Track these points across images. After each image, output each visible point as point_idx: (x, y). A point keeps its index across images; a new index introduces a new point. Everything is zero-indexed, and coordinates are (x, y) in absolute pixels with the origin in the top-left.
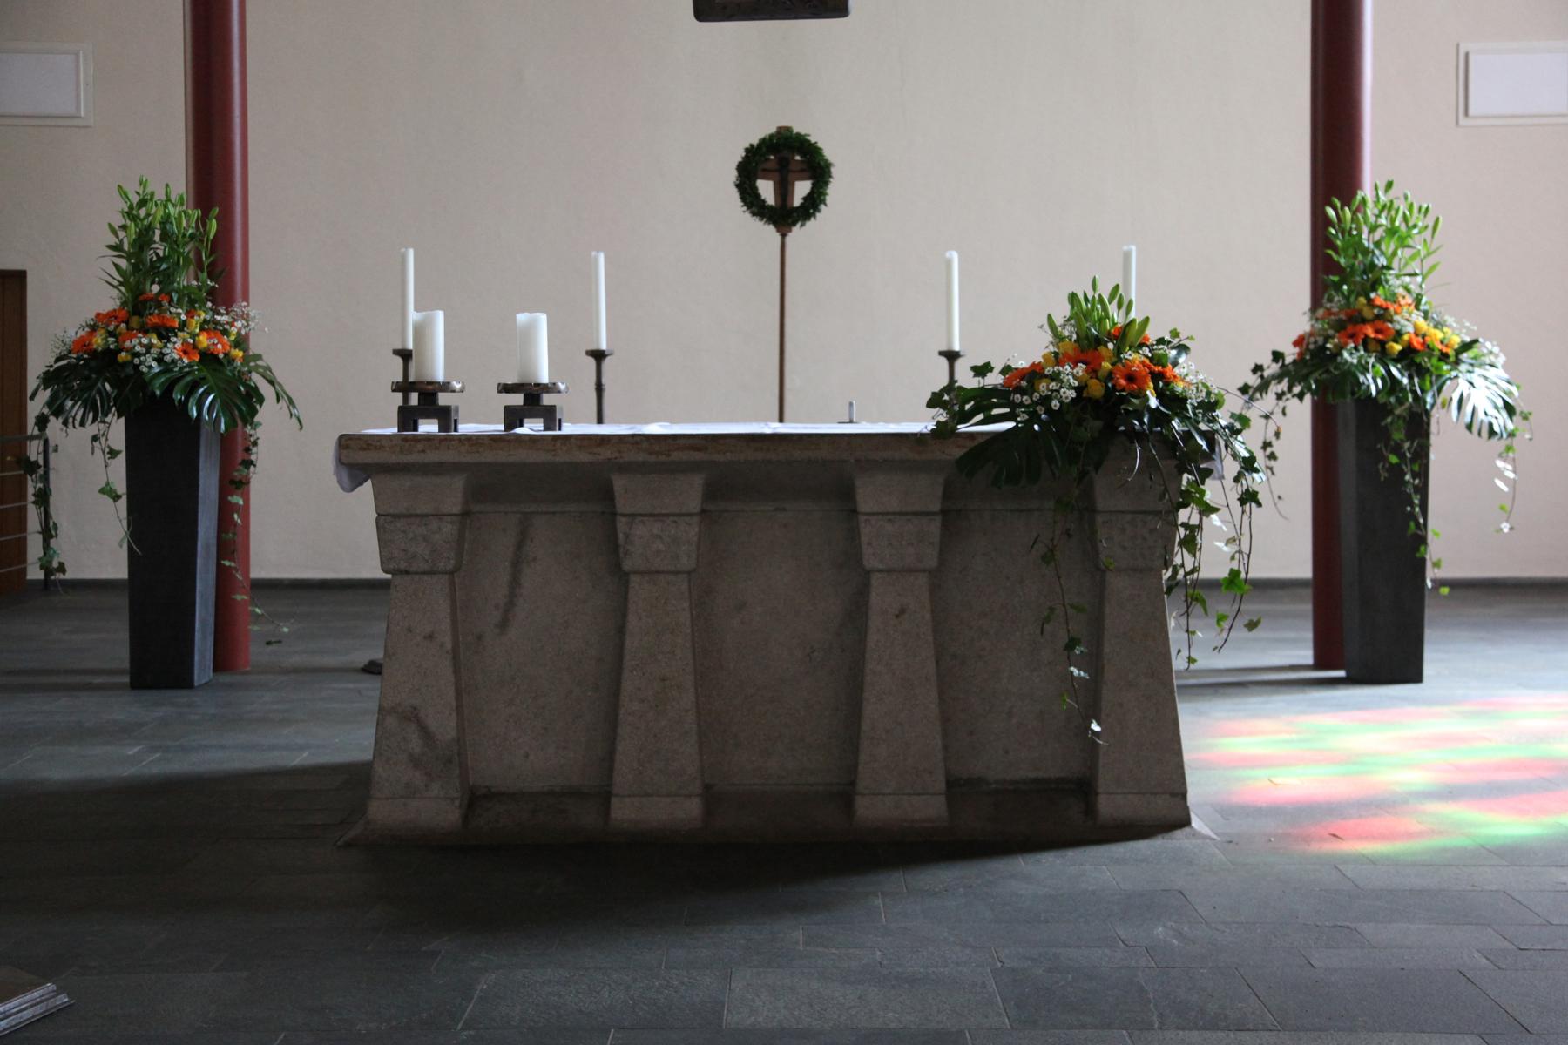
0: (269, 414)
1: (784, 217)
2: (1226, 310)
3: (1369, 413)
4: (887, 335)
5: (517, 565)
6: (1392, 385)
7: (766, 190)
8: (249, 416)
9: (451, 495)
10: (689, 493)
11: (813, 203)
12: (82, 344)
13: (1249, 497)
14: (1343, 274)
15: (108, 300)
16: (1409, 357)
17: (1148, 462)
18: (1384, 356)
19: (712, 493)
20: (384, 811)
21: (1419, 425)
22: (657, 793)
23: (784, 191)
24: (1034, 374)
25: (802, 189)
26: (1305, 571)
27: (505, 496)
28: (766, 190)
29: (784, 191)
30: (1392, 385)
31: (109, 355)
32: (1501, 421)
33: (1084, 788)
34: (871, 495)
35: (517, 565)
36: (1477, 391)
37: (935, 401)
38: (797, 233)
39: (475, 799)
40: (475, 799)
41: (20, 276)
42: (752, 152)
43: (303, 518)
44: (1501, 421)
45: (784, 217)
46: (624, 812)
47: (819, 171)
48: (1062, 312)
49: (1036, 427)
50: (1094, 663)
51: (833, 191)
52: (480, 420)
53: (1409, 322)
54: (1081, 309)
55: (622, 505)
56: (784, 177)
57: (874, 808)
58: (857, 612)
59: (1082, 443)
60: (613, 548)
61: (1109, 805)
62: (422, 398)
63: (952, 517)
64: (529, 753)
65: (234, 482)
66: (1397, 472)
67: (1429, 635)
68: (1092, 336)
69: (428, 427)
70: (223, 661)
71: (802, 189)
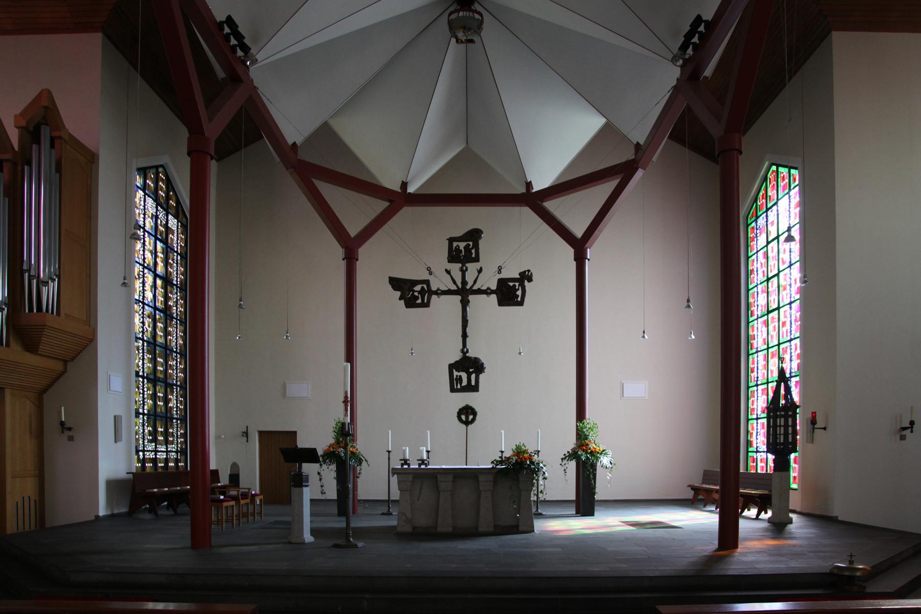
0: (364, 463)
1: (467, 423)
2: (551, 447)
3: (584, 462)
4: (485, 450)
5: (421, 489)
6: (587, 458)
7: (463, 417)
8: (360, 464)
9: (410, 478)
10: (450, 477)
11: (473, 420)
12: (328, 450)
13: (545, 478)
14: (581, 436)
15: (332, 441)
16: (592, 453)
17: (527, 473)
18: (587, 453)
19: (454, 477)
20: (399, 529)
21: (594, 466)
22: (445, 526)
23: (467, 418)
24: (509, 458)
25: (471, 417)
26: (574, 498)
27: (418, 479)
28: (463, 417)
29: (467, 418)
30: (587, 458)
31: (334, 452)
32: (609, 465)
33: (517, 526)
34: (481, 478)
35: (421, 489)
36: (605, 460)
37: (492, 462)
38: (470, 426)
39: (414, 528)
40: (414, 528)
41: (295, 432)
42: (460, 410)
43: (373, 482)
44: (609, 465)
45: (467, 423)
46: (439, 529)
47: (474, 413)
48: (514, 448)
49: (222, 497)
50: (519, 505)
51: (478, 417)
52: (414, 466)
53: (592, 446)
54: (518, 447)
55: (439, 479)
56: (467, 415)
57: (481, 529)
58: (479, 497)
59: (519, 470)
60: (437, 487)
61: (521, 529)
62: (405, 462)
63: (495, 482)
64: (423, 521)
65: (356, 477)
66: (589, 475)
67: (596, 508)
68: (519, 452)
69: (406, 467)
70: (354, 513)
71: (471, 417)
